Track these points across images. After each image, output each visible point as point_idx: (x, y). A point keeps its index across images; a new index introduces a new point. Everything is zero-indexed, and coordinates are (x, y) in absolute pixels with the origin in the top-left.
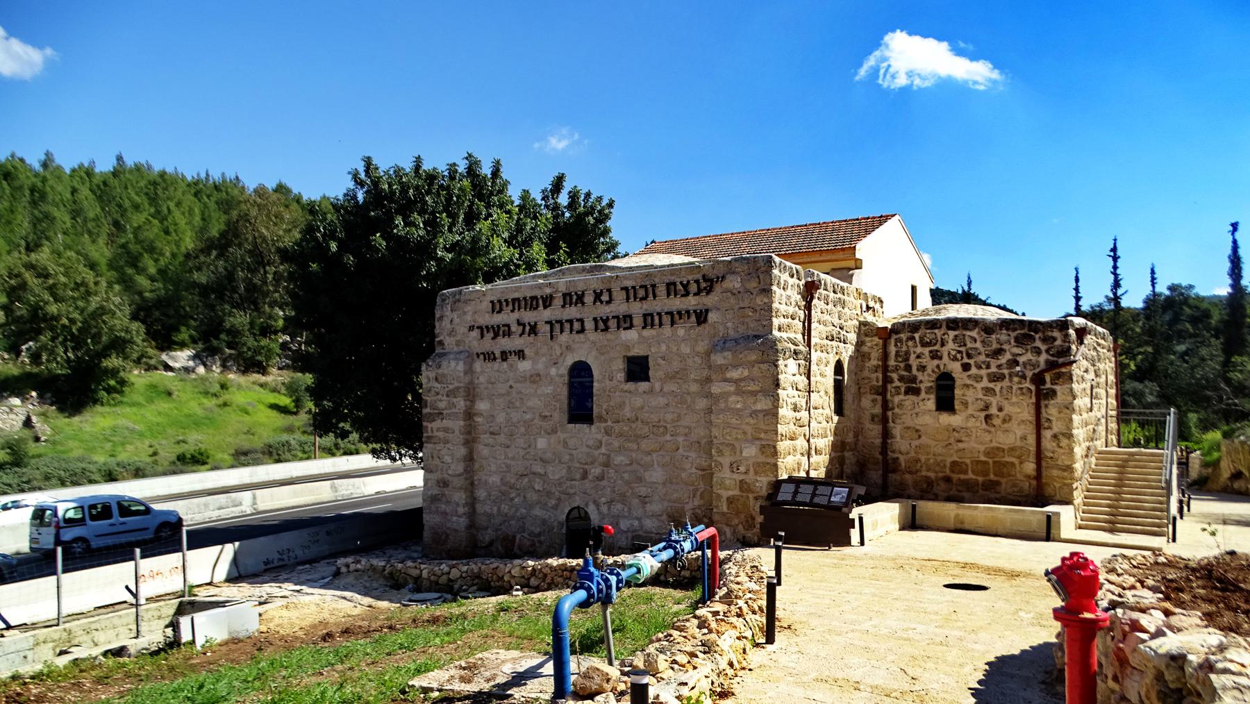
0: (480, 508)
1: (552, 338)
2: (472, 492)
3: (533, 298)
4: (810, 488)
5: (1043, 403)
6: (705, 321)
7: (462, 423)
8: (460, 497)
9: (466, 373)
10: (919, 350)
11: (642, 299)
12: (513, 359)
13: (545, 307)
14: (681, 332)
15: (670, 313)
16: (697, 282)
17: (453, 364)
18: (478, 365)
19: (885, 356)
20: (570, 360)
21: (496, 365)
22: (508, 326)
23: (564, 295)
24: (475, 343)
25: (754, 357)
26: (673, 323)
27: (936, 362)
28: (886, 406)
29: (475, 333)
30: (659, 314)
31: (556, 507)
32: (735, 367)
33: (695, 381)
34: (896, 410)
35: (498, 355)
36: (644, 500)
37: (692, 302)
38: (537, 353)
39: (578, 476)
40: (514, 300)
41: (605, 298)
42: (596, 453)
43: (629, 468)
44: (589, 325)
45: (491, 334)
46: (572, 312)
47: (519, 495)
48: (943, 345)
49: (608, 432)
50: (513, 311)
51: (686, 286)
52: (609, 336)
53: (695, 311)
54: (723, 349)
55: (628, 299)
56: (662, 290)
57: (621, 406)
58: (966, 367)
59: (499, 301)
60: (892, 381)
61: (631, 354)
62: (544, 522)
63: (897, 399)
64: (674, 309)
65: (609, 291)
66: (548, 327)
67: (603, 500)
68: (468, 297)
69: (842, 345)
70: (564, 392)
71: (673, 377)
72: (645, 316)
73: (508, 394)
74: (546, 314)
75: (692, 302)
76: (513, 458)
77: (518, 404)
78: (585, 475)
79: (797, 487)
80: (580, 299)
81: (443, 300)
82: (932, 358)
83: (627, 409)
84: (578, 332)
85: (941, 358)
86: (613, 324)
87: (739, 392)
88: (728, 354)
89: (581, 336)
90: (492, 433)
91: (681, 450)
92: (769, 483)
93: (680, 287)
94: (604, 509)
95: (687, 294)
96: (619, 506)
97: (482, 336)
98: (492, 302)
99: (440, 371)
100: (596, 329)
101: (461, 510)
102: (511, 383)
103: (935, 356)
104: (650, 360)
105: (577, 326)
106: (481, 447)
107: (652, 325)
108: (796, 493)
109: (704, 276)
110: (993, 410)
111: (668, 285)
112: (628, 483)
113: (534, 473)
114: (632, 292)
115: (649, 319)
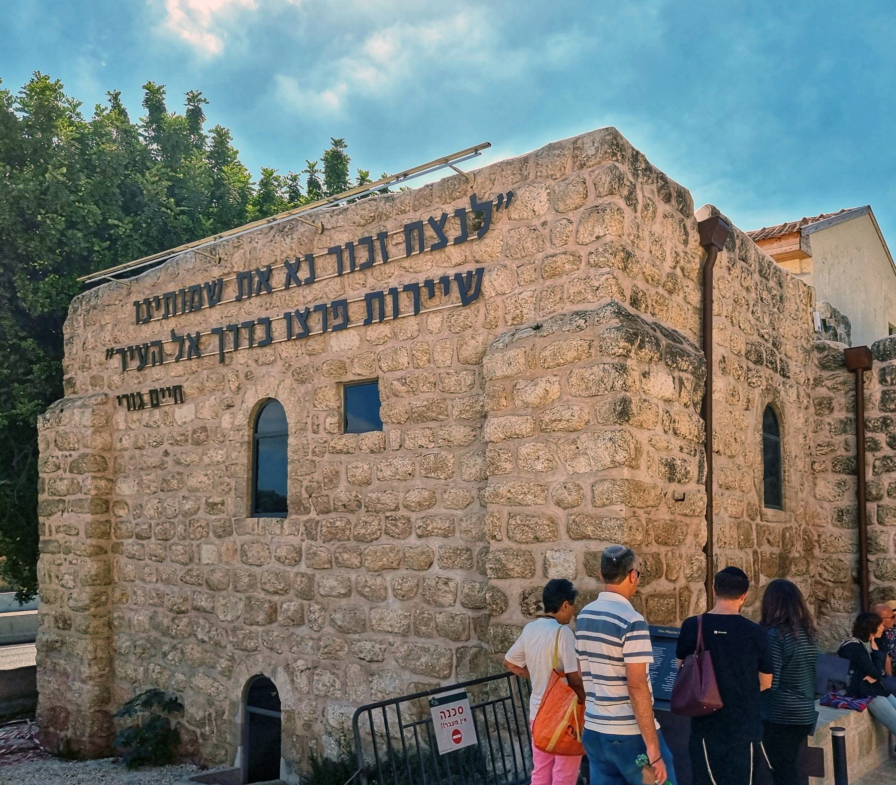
1: (222, 360)
6: (478, 293)
7: (89, 517)
14: (434, 322)
15: (412, 288)
18: (121, 416)
21: (145, 415)
28: (862, 494)
30: (394, 292)
34: (886, 501)
38: (201, 390)
39: (261, 617)
42: (292, 571)
43: (344, 602)
47: (174, 648)
50: (166, 317)
52: (314, 344)
57: (332, 479)
60: (876, 447)
61: (350, 377)
73: (161, 466)
75: (453, 260)
83: (343, 485)
87: (542, 430)
89: (268, 350)
90: (139, 537)
91: (436, 568)
93: (430, 232)
95: (442, 245)
96: (327, 678)
102: (166, 446)
112: (343, 631)
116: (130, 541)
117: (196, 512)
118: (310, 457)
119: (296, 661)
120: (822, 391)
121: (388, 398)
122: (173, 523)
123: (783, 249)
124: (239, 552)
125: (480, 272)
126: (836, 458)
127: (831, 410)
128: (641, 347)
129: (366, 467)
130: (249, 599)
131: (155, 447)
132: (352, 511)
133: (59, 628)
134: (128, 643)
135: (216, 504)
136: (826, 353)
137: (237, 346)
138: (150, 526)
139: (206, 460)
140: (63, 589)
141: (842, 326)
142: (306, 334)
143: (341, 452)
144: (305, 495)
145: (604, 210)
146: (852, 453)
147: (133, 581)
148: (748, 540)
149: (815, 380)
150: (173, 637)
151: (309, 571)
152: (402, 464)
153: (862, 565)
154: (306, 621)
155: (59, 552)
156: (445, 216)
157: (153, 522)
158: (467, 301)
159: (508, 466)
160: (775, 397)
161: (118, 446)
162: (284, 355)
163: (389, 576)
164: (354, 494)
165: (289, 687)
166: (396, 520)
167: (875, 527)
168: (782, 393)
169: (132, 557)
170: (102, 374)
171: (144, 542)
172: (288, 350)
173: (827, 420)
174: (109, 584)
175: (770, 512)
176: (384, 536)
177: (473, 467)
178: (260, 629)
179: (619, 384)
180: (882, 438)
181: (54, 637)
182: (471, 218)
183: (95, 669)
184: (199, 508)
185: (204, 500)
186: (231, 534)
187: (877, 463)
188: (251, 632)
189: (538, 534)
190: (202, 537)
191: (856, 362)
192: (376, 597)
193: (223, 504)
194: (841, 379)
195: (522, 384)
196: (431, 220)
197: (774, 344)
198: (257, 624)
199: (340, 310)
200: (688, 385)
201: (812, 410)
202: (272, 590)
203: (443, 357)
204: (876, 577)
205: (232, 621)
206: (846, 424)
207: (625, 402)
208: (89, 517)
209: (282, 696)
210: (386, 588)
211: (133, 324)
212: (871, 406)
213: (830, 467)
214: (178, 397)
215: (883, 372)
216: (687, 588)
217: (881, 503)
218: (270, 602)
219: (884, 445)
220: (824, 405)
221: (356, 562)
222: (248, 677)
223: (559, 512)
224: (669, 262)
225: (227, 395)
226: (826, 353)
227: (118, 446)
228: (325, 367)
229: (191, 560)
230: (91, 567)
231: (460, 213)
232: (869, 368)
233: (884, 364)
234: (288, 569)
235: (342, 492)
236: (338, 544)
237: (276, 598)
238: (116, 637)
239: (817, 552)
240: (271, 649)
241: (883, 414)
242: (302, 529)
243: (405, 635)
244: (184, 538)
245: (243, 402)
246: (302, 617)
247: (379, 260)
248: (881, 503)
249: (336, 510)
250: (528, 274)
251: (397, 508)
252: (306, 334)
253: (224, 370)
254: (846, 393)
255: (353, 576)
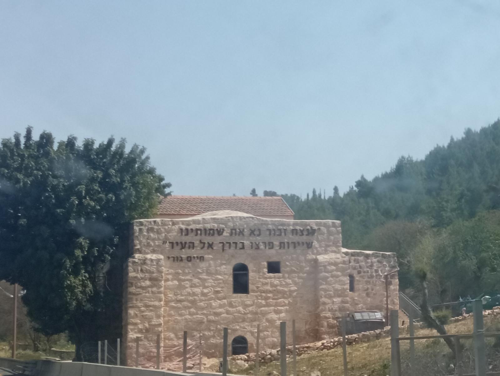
1: (223, 250)
5: (388, 286)
11: (278, 235)
15: (294, 243)
20: (235, 262)
37: (305, 238)
58: (359, 273)
70: (231, 279)
75: (305, 238)
89: (242, 250)
95: (303, 235)
107: (284, 248)
110: (370, 290)
115: (282, 245)
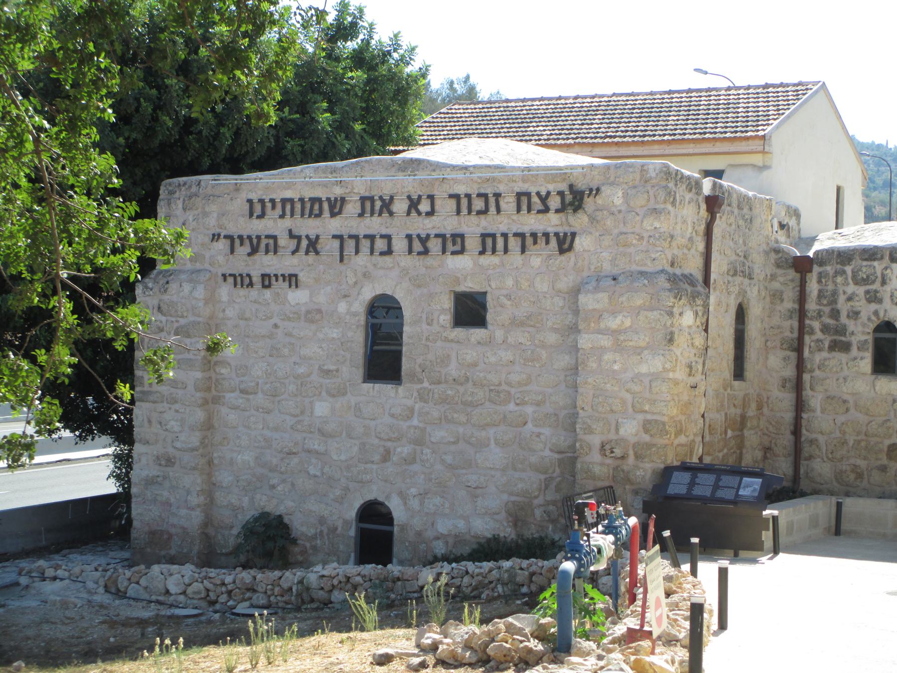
0: (220, 497)
1: (342, 260)
2: (210, 475)
3: (313, 200)
4: (710, 478)
6: (570, 248)
7: (199, 375)
8: (192, 481)
9: (207, 302)
10: (851, 288)
11: (479, 213)
12: (280, 286)
13: (333, 215)
14: (536, 261)
15: (521, 236)
16: (561, 194)
17: (187, 287)
18: (225, 291)
19: (802, 298)
20: (368, 293)
21: (254, 293)
22: (275, 238)
23: (363, 199)
24: (221, 259)
25: (639, 302)
26: (523, 250)
27: (873, 306)
28: (800, 366)
29: (222, 245)
30: (505, 236)
31: (340, 500)
32: (614, 313)
33: (555, 330)
34: (817, 373)
35: (256, 279)
36: (474, 492)
37: (552, 222)
38: (317, 280)
39: (377, 458)
40: (284, 201)
41: (424, 207)
42: (404, 425)
43: (453, 448)
44: (400, 245)
45: (247, 249)
46: (375, 224)
47: (284, 481)
48: (884, 283)
49: (423, 397)
50: (282, 216)
51: (544, 199)
52: (429, 260)
53: (557, 234)
54: (597, 289)
55: (458, 212)
56: (508, 203)
57: (445, 360)
59: (262, 201)
60: (812, 332)
61: (462, 288)
62: (322, 520)
63: (818, 357)
64: (526, 229)
65: (431, 198)
66: (336, 243)
67: (414, 491)
68: (209, 191)
69: (746, 281)
71: (522, 324)
72: (484, 236)
73: (271, 336)
74: (335, 225)
75: (552, 222)
76: (276, 429)
77: (286, 351)
78: (386, 456)
79: (694, 477)
80: (387, 206)
81: (171, 193)
82: (869, 301)
83: (453, 365)
84: (382, 254)
85: (880, 301)
86: (435, 245)
87: (619, 347)
88: (603, 296)
89: (387, 258)
90: (243, 391)
91: (530, 425)
92: (654, 472)
93: (535, 199)
94: (415, 504)
95: (546, 210)
96: (438, 500)
97: (232, 251)
98: (250, 201)
99: (166, 297)
100: (410, 251)
101: (195, 500)
102: (276, 320)
103: (873, 298)
104: (489, 298)
105: (380, 244)
106: (224, 410)
108: (692, 484)
109: (571, 187)
111: (519, 195)
112: (451, 467)
113: (309, 451)
114: (464, 202)
115: (489, 241)
116: (232, 395)
117: (309, 376)
118: (423, 342)
119: (409, 489)
120: (776, 285)
121: (495, 307)
122: (284, 383)
123: (750, 148)
124: (353, 409)
125: (574, 235)
126: (783, 339)
127: (782, 301)
128: (680, 299)
129: (475, 354)
130: (364, 444)
131: (264, 320)
132: (461, 384)
133: (160, 465)
134: (230, 478)
135: (332, 371)
136: (780, 255)
137: (357, 252)
138: (257, 384)
139: (321, 336)
140: (166, 433)
141: (794, 218)
142: (426, 252)
143: (452, 341)
144: (418, 370)
145: (661, 213)
146: (796, 335)
147: (235, 427)
148: (722, 405)
149: (771, 275)
150: (282, 473)
151: (421, 425)
152: (506, 355)
153: (798, 420)
154: (418, 460)
155: (162, 402)
156: (548, 193)
157: (260, 381)
158: (562, 251)
159: (594, 365)
160: (744, 296)
161: (221, 315)
162: (402, 264)
163: (491, 431)
164: (463, 372)
165: (402, 507)
166: (498, 392)
167: (807, 392)
168: (749, 292)
169: (235, 408)
170: (203, 253)
171: (251, 397)
172: (407, 261)
173: (779, 308)
174: (209, 429)
175: (736, 383)
176: (487, 403)
177: (564, 361)
178: (375, 467)
179: (669, 323)
180: (816, 325)
181: (155, 473)
182: (569, 198)
183: (202, 498)
184: (311, 373)
185: (317, 367)
186: (344, 394)
187: (813, 344)
188: (365, 469)
189: (614, 408)
190: (315, 395)
191: (802, 265)
192: (482, 445)
193: (337, 371)
194: (790, 277)
195: (605, 315)
196: (538, 194)
197: (745, 257)
198: (372, 462)
199: (459, 240)
200: (700, 314)
201: (768, 299)
202: (386, 437)
203: (542, 286)
204: (807, 430)
205: (346, 461)
206: (792, 312)
207: (672, 333)
208: (199, 375)
209: (395, 515)
210: (489, 439)
211: (243, 216)
212: (810, 300)
213: (779, 345)
214: (293, 283)
215: (820, 276)
216: (693, 441)
217: (814, 374)
218: (384, 447)
219: (817, 330)
220: (776, 296)
221: (463, 419)
222: (362, 502)
223: (628, 397)
224: (690, 230)
225: (343, 287)
226: (780, 255)
227: (221, 315)
228: (441, 279)
229: (302, 413)
230: (200, 415)
231: (561, 194)
232: (811, 271)
233: (821, 269)
234: (401, 423)
235: (453, 370)
236: (447, 407)
237: (389, 444)
238: (217, 473)
239: (765, 410)
240: (386, 481)
241: (818, 307)
242: (415, 394)
243: (504, 470)
244: (296, 395)
245: (359, 294)
246: (414, 458)
247: (493, 209)
248: (814, 374)
249: (446, 382)
250: (607, 241)
251: (500, 384)
252: (426, 252)
253: (342, 267)
254: (794, 288)
255: (461, 430)
